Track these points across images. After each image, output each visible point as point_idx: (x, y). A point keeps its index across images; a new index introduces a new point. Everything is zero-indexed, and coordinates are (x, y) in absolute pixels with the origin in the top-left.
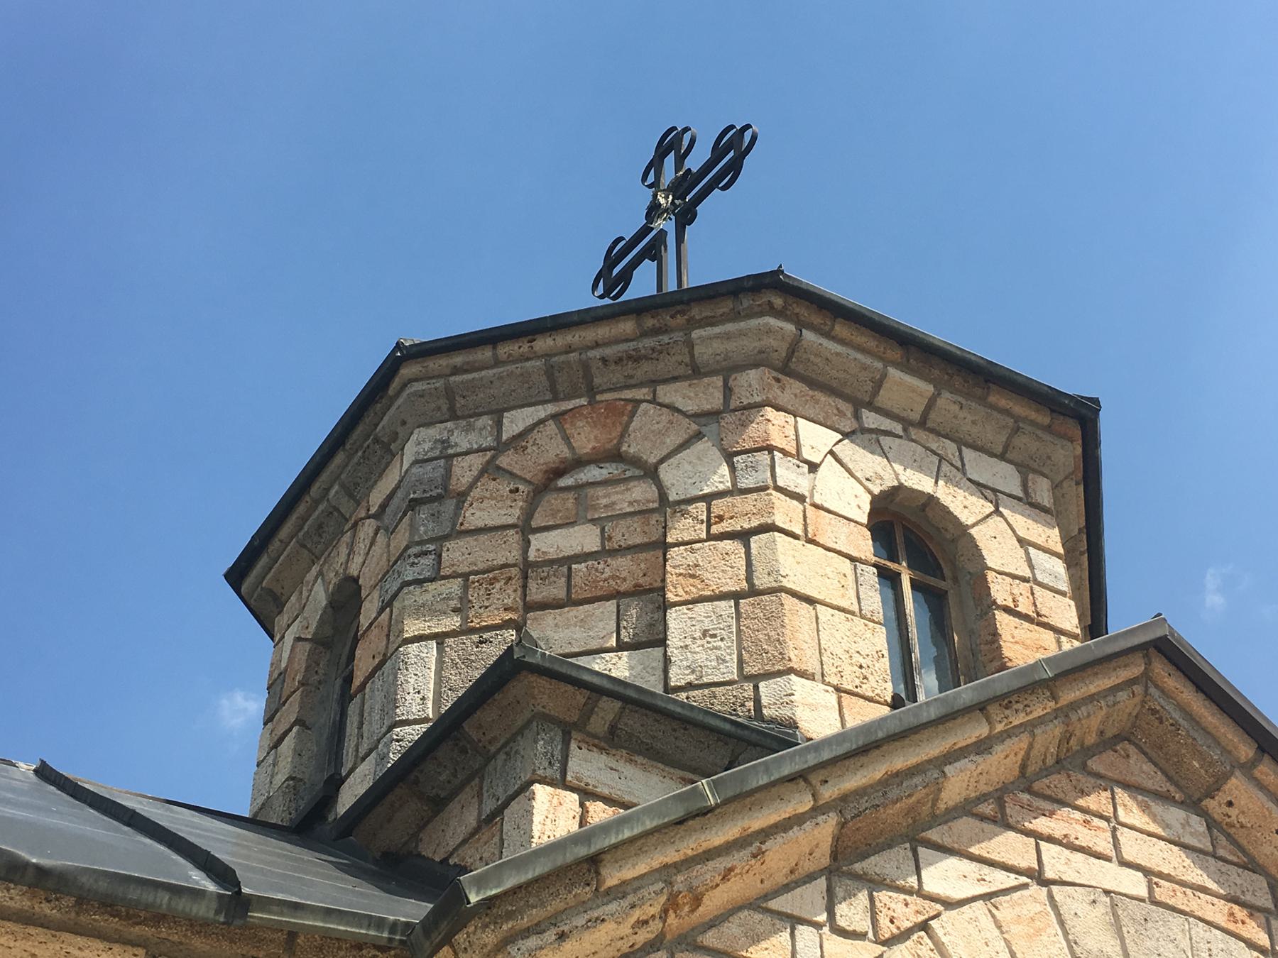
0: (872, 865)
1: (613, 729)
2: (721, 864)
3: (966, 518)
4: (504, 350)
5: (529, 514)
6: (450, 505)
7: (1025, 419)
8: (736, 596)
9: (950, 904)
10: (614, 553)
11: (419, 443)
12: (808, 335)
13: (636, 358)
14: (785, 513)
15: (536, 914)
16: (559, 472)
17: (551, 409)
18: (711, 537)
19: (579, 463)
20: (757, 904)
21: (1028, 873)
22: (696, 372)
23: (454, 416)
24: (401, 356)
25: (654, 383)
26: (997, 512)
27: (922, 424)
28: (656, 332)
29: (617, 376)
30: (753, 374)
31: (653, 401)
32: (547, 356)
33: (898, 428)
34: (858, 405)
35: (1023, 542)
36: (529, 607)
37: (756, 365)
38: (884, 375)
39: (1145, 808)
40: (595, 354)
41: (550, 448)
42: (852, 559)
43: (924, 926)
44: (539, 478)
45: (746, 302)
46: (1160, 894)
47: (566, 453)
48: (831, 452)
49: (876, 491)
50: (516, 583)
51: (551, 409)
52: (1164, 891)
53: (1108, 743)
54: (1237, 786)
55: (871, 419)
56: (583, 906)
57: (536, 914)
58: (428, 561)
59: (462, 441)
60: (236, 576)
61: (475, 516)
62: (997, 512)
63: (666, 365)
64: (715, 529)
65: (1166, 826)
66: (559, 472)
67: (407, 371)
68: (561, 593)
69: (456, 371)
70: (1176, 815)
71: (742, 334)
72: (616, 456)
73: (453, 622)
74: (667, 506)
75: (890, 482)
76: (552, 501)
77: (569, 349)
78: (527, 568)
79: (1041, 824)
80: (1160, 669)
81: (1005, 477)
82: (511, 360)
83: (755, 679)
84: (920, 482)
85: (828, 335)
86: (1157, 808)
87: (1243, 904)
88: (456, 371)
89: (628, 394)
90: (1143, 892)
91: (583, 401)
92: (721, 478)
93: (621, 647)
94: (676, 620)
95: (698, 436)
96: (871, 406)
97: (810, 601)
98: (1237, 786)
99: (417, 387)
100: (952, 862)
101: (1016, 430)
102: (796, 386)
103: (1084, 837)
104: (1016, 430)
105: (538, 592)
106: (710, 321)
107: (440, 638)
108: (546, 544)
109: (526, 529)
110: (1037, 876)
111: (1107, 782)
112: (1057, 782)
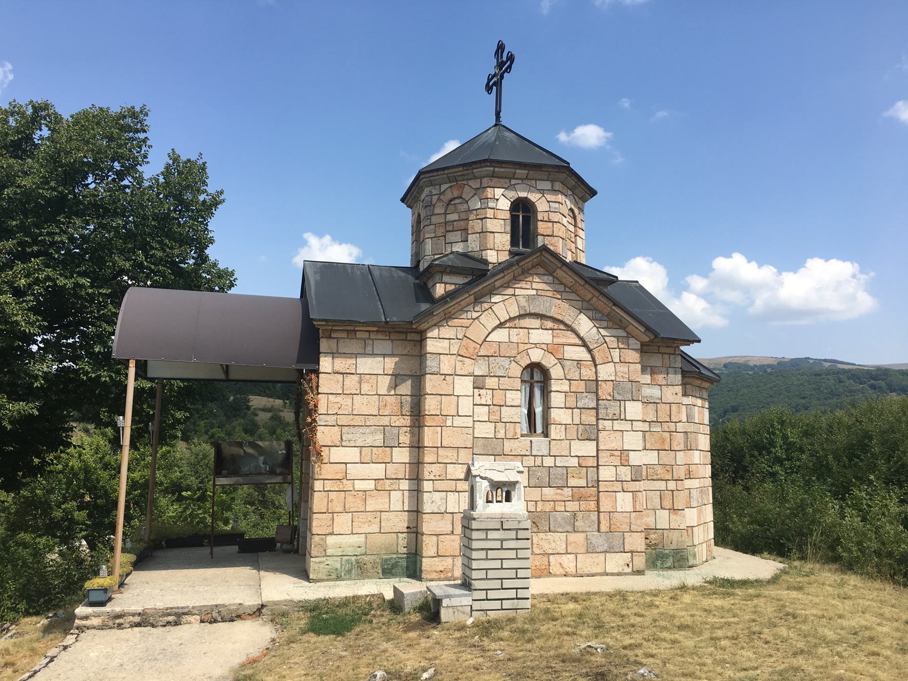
0: (482, 300)
1: (451, 271)
2: (453, 307)
3: (534, 200)
4: (439, 173)
5: (446, 210)
6: (432, 207)
7: (551, 171)
8: (480, 233)
9: (496, 303)
10: (460, 220)
11: (426, 191)
12: (496, 169)
13: (463, 175)
14: (490, 213)
15: (423, 321)
16: (451, 201)
17: (449, 185)
18: (477, 219)
19: (455, 198)
20: (461, 310)
21: (512, 295)
22: (475, 178)
23: (432, 185)
24: (421, 173)
25: (468, 180)
26: (543, 196)
27: (527, 178)
28: (467, 170)
29: (461, 178)
30: (485, 179)
31: (467, 185)
32: (447, 174)
33: (520, 182)
34: (510, 179)
35: (548, 202)
36: (447, 231)
37: (486, 177)
38: (515, 172)
39: (539, 278)
40: (455, 174)
41: (449, 195)
42: (504, 220)
43: (491, 308)
44: (447, 202)
45: (483, 165)
46: (538, 293)
47: (452, 197)
48: (502, 194)
49: (512, 200)
50: (444, 227)
51: (449, 185)
52: (540, 293)
53: (533, 267)
54: (558, 271)
55: (513, 182)
56: (431, 318)
57: (423, 321)
58: (429, 221)
59: (434, 192)
60: (403, 200)
61: (437, 211)
62: (543, 196)
63: (470, 177)
64: (477, 217)
65: (543, 280)
66: (451, 201)
67: (421, 177)
68: (452, 229)
69: (431, 177)
70: (546, 278)
71: (482, 171)
72: (461, 197)
73: (433, 235)
74: (469, 211)
75: (516, 197)
76: (450, 207)
77: (451, 173)
78: (446, 223)
79: (516, 286)
80: (544, 253)
81: (547, 185)
82: (440, 175)
83: (482, 250)
84: (523, 194)
85: (502, 167)
86: (542, 277)
87: (556, 291)
88: (431, 177)
89: (463, 182)
90: (535, 294)
91: (455, 183)
92: (479, 205)
93: (462, 241)
94: (470, 237)
95: (475, 194)
96: (514, 178)
97: (493, 232)
98: (558, 271)
99: (425, 180)
100: (498, 296)
101: (549, 174)
102: (495, 180)
103: (524, 286)
104: (549, 174)
105: (448, 229)
106: (477, 168)
107: (432, 238)
108: (451, 217)
109: (445, 214)
110: (514, 295)
111: (532, 275)
112: (521, 277)
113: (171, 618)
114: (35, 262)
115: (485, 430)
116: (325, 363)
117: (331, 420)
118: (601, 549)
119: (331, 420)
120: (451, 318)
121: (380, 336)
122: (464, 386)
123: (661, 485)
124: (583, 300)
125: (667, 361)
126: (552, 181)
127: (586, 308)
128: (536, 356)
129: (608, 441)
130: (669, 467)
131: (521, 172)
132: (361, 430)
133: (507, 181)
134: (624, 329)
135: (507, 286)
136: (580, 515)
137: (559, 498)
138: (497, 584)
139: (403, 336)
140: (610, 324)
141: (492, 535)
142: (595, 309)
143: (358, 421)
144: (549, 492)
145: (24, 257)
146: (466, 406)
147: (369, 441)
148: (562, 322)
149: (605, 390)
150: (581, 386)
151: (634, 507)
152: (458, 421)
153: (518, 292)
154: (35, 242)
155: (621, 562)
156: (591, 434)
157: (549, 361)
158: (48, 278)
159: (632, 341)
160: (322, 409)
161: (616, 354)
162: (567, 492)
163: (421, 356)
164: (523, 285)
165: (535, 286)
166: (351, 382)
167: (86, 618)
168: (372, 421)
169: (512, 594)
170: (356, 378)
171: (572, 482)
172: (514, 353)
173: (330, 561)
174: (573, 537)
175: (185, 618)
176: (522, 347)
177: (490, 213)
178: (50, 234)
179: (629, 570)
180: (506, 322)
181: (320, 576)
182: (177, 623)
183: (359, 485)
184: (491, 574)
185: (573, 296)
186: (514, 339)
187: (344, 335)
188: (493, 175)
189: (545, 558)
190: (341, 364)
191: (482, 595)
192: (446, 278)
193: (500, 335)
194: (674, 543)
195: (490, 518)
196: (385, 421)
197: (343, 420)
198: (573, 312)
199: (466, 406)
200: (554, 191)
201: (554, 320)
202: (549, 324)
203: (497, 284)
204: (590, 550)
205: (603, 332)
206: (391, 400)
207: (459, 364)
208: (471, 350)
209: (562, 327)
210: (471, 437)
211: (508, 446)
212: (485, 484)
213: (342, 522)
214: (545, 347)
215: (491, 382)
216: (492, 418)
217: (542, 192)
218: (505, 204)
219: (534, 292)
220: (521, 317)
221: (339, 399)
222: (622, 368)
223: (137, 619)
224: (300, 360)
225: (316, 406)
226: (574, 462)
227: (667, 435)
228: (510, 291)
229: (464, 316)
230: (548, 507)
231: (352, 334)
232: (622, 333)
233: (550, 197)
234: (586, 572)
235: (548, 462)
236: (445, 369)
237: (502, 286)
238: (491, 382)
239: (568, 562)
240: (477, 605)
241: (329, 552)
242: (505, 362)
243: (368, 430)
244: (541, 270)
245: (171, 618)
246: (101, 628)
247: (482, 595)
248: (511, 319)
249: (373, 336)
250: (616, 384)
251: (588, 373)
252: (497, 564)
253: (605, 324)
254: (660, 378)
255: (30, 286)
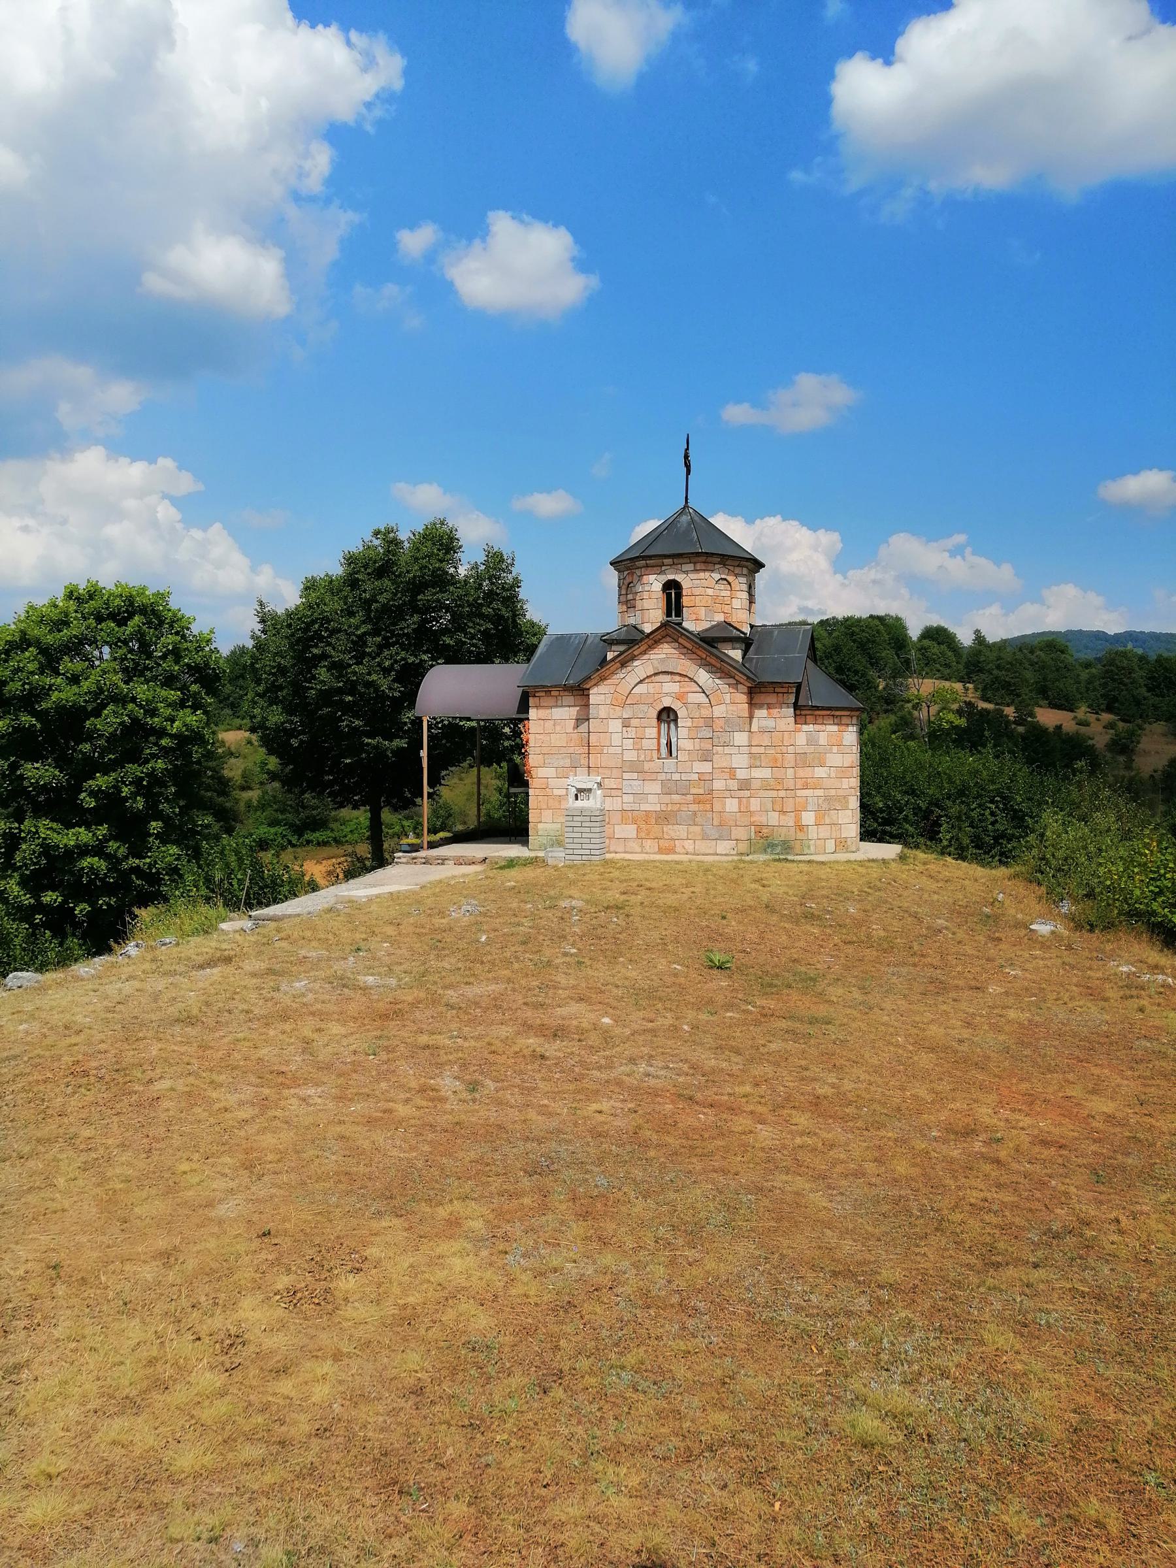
55: (663, 568)
78: (627, 601)
81: (690, 567)
84: (671, 577)
113: (439, 861)
114: (393, 649)
115: (631, 756)
116: (533, 713)
117: (538, 750)
118: (713, 837)
119: (538, 750)
120: (605, 679)
121: (566, 693)
122: (615, 726)
123: (774, 794)
124: (702, 659)
125: (780, 699)
126: (695, 563)
127: (705, 664)
128: (667, 702)
129: (720, 761)
130: (779, 780)
131: (666, 561)
132: (556, 756)
133: (659, 568)
134: (734, 678)
135: (644, 652)
136: (699, 814)
137: (683, 801)
138: (579, 846)
139: (581, 693)
140: (723, 675)
141: (576, 818)
142: (710, 664)
143: (554, 751)
144: (676, 798)
145: (387, 645)
146: (616, 739)
147: (562, 763)
148: (686, 676)
149: (718, 724)
150: (701, 722)
151: (740, 808)
152: (611, 750)
153: (652, 657)
154: (393, 635)
155: (728, 847)
156: (706, 757)
157: (676, 706)
158: (403, 659)
159: (740, 686)
160: (531, 743)
161: (727, 697)
162: (690, 798)
163: (587, 705)
164: (656, 651)
165: (665, 651)
166: (549, 724)
167: (399, 858)
168: (563, 750)
169: (588, 852)
170: (552, 722)
171: (693, 791)
172: (651, 701)
173: (540, 839)
174: (693, 828)
175: (446, 862)
176: (656, 696)
177: (645, 596)
178: (401, 629)
179: (735, 852)
180: (644, 679)
181: (535, 848)
182: (442, 864)
183: (556, 792)
184: (576, 840)
185: (694, 656)
186: (651, 691)
187: (543, 694)
188: (647, 566)
189: (672, 842)
190: (543, 713)
191: (571, 852)
192: (614, 648)
193: (641, 689)
194: (783, 835)
195: (575, 809)
196: (571, 750)
197: (545, 750)
198: (694, 667)
199: (616, 739)
200: (696, 571)
201: (681, 675)
202: (677, 678)
203: (636, 653)
204: (705, 837)
205: (718, 681)
206: (575, 736)
207: (612, 711)
208: (620, 701)
209: (687, 679)
210: (620, 760)
211: (647, 766)
212: (574, 789)
213: (547, 815)
214: (673, 695)
215: (634, 722)
216: (636, 747)
217: (686, 572)
218: (657, 587)
219: (664, 656)
220: (656, 674)
221: (541, 737)
222: (732, 708)
223: (423, 860)
224: (518, 712)
225: (527, 742)
226: (696, 777)
227: (779, 756)
228: (646, 657)
229: (615, 677)
230: (676, 808)
231: (548, 692)
232: (732, 681)
233: (692, 576)
234: (702, 852)
235: (676, 777)
236: (603, 714)
237: (641, 654)
238: (634, 722)
239: (689, 845)
240: (568, 857)
241: (540, 833)
242: (645, 708)
243: (560, 756)
244: (668, 639)
245: (439, 861)
246: (407, 863)
247: (571, 852)
248: (648, 677)
249: (562, 694)
250: (727, 720)
251: (706, 712)
252: (579, 835)
253: (719, 675)
254: (775, 712)
255: (392, 665)
